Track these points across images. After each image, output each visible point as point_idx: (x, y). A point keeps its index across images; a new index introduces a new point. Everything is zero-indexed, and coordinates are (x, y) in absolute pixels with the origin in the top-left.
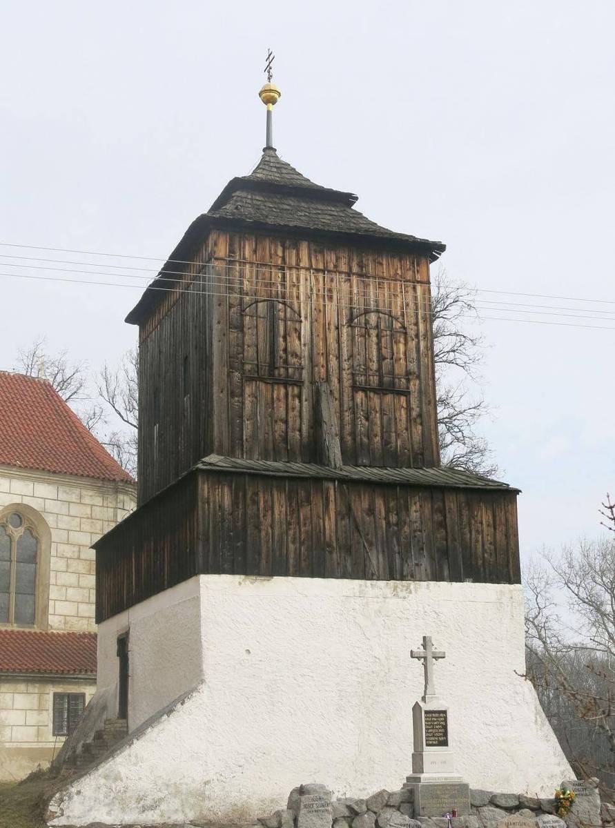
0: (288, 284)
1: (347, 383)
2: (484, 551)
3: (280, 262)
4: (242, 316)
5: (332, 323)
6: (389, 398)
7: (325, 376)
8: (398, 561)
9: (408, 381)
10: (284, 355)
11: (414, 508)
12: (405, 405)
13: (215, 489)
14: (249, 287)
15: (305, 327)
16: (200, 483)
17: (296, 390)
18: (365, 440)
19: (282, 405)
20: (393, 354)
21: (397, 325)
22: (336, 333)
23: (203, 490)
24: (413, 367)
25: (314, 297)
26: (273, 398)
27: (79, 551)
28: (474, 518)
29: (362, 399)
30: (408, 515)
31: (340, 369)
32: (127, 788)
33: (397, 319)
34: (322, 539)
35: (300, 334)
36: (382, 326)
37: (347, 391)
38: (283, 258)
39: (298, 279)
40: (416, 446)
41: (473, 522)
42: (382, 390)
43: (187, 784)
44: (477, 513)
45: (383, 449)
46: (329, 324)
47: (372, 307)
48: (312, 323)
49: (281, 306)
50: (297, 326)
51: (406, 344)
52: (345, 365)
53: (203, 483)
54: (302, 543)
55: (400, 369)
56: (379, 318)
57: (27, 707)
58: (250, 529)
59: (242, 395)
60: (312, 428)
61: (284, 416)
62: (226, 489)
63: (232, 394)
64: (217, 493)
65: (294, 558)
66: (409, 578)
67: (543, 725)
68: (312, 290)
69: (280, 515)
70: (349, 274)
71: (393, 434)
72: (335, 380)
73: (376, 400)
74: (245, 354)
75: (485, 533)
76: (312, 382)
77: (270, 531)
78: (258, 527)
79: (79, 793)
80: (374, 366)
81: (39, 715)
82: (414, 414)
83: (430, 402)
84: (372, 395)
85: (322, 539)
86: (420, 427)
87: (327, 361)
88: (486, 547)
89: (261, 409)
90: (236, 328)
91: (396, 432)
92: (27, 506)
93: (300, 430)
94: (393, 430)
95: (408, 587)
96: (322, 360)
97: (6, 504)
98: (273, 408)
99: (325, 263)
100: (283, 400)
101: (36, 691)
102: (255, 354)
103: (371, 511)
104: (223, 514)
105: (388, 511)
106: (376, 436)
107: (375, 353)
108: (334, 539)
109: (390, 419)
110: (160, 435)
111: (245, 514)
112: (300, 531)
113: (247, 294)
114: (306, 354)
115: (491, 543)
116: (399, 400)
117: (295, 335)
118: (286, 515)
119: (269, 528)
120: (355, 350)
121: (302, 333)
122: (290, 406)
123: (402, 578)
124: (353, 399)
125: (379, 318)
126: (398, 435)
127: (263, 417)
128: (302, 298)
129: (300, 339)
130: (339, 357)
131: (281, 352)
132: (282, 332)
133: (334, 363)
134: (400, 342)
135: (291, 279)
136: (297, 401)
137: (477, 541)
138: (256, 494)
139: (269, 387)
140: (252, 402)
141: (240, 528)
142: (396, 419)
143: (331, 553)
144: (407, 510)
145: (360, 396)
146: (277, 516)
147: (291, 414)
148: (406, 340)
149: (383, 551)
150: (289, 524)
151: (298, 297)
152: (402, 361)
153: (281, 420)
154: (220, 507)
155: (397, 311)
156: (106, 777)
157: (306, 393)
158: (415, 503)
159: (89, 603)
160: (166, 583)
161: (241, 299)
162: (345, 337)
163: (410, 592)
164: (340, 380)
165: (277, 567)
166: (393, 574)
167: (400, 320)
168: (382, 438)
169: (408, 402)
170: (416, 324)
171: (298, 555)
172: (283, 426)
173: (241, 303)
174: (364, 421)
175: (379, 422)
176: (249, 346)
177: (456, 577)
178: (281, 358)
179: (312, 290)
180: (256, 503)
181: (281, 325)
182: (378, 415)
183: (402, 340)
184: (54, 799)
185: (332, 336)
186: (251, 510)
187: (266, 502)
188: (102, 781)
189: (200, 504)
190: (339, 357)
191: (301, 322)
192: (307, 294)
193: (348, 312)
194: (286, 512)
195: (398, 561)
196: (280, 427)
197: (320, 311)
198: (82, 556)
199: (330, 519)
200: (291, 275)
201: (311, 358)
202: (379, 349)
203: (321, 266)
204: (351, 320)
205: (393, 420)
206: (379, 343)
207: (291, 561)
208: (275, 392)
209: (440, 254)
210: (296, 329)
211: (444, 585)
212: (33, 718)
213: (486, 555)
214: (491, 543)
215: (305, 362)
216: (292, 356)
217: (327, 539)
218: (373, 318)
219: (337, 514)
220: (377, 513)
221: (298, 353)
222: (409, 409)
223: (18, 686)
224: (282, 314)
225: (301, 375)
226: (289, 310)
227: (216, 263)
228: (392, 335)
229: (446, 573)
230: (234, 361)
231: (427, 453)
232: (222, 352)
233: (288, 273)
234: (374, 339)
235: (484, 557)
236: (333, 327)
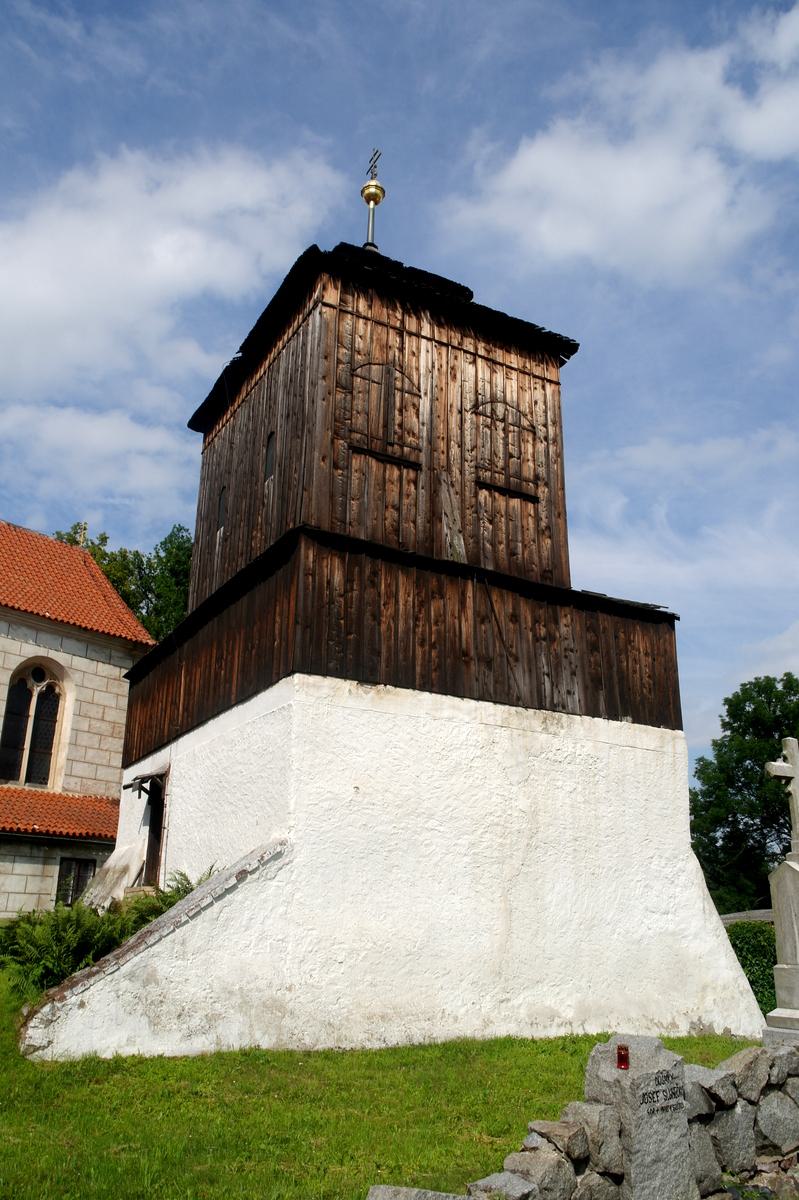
0: (406, 352)
1: (469, 476)
2: (643, 685)
3: (398, 324)
4: (352, 375)
5: (454, 405)
6: (515, 502)
7: (445, 464)
8: (548, 685)
9: (537, 486)
10: (399, 431)
11: (564, 621)
12: (532, 513)
13: (323, 558)
14: (361, 346)
15: (425, 404)
16: (303, 545)
17: (412, 474)
18: (488, 546)
19: (396, 490)
20: (521, 454)
21: (525, 423)
22: (459, 416)
23: (307, 557)
24: (542, 471)
25: (436, 372)
26: (384, 478)
27: (104, 713)
28: (630, 643)
29: (486, 498)
30: (558, 629)
31: (463, 459)
32: (164, 997)
33: (525, 416)
34: (457, 645)
35: (418, 410)
36: (510, 420)
37: (470, 486)
38: (403, 322)
39: (418, 349)
40: (544, 562)
41: (629, 648)
42: (509, 492)
43: (259, 990)
44: (634, 637)
45: (509, 560)
46: (451, 406)
47: (499, 395)
48: (432, 401)
49: (398, 374)
50: (416, 400)
51: (534, 446)
52: (468, 456)
53: (307, 549)
54: (433, 646)
55: (528, 470)
56: (506, 409)
57: (30, 873)
58: (368, 619)
59: (348, 467)
60: (429, 522)
61: (396, 502)
62: (337, 562)
63: (336, 466)
64: (325, 564)
65: (422, 665)
66: (561, 709)
67: (711, 914)
68: (433, 363)
69: (405, 605)
70: (475, 355)
71: (520, 545)
72: (456, 471)
73: (501, 501)
74: (353, 420)
75: (643, 663)
76: (431, 469)
77: (392, 625)
78: (376, 617)
79: (82, 1005)
80: (501, 463)
81: (42, 881)
82: (543, 524)
83: (559, 515)
84: (497, 495)
85: (457, 645)
86: (549, 541)
87: (448, 447)
88: (644, 681)
89: (372, 489)
90: (344, 388)
91: (523, 543)
92: (52, 660)
93: (414, 522)
94: (520, 538)
95: (559, 720)
96: (442, 445)
97: (30, 656)
98: (385, 490)
99: (449, 338)
100: (397, 484)
101: (41, 854)
102: (366, 423)
103: (515, 618)
104: (331, 594)
105: (536, 621)
106: (501, 543)
107: (501, 448)
108: (472, 647)
109: (516, 527)
110: (225, 539)
111: (361, 598)
112: (430, 628)
113: (359, 353)
114: (425, 434)
115: (649, 677)
116: (526, 506)
117: (412, 411)
118: (414, 607)
119: (392, 622)
120: (480, 442)
121: (421, 410)
122: (404, 492)
123: (554, 708)
124: (476, 495)
125: (506, 409)
126: (525, 546)
127: (372, 500)
128: (422, 370)
129: (418, 417)
130: (461, 445)
131: (396, 427)
132: (398, 404)
133: (455, 450)
134: (528, 441)
135: (410, 346)
136: (412, 487)
137: (635, 672)
138: (375, 573)
139: (381, 465)
140: (359, 479)
141: (354, 617)
142: (523, 527)
143: (467, 663)
144: (556, 622)
145: (484, 494)
146: (401, 607)
147: (406, 501)
148: (534, 440)
149: (530, 671)
150: (416, 619)
151: (418, 369)
152: (531, 464)
153: (393, 507)
154: (329, 582)
155: (524, 407)
156: (131, 976)
157: (422, 478)
158: (566, 616)
159: (120, 738)
160: (233, 697)
161: (352, 357)
162: (467, 425)
163: (562, 727)
164: (462, 472)
165: (403, 677)
166: (538, 701)
167: (529, 417)
168: (508, 545)
169: (536, 510)
170: (545, 426)
171: (427, 661)
172: (396, 515)
173: (351, 361)
174: (487, 524)
175: (504, 528)
176: (358, 413)
177: (613, 715)
178: (395, 433)
179: (433, 363)
180: (374, 585)
181: (398, 395)
182: (503, 519)
183: (530, 439)
184: (39, 1015)
185: (454, 419)
186: (369, 594)
187: (388, 586)
188: (125, 984)
189: (301, 575)
190: (461, 445)
191: (420, 397)
192: (427, 367)
193: (473, 397)
194: (414, 603)
195: (548, 685)
196: (391, 514)
197: (442, 389)
198: (107, 718)
199: (466, 620)
200: (410, 343)
201: (430, 442)
202: (506, 444)
203: (445, 340)
204: (476, 406)
205: (520, 528)
206: (506, 438)
207: (418, 669)
208: (388, 472)
209: (568, 358)
210: (414, 405)
211: (600, 722)
212: (34, 885)
213: (645, 691)
214: (649, 677)
215: (424, 444)
216: (408, 433)
217: (464, 645)
218: (500, 409)
219: (476, 613)
220: (522, 620)
221: (416, 431)
222: (537, 519)
223: (22, 848)
224: (398, 384)
225: (418, 456)
226: (406, 380)
227: (325, 309)
228: (520, 433)
229: (602, 706)
230: (339, 425)
231: (555, 573)
232: (325, 416)
233: (407, 339)
234: (502, 434)
235: (642, 692)
236: (455, 410)
